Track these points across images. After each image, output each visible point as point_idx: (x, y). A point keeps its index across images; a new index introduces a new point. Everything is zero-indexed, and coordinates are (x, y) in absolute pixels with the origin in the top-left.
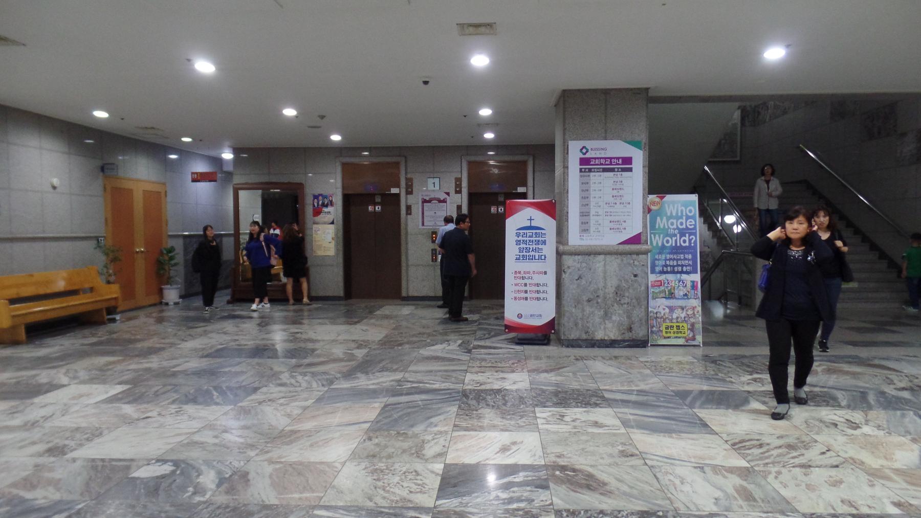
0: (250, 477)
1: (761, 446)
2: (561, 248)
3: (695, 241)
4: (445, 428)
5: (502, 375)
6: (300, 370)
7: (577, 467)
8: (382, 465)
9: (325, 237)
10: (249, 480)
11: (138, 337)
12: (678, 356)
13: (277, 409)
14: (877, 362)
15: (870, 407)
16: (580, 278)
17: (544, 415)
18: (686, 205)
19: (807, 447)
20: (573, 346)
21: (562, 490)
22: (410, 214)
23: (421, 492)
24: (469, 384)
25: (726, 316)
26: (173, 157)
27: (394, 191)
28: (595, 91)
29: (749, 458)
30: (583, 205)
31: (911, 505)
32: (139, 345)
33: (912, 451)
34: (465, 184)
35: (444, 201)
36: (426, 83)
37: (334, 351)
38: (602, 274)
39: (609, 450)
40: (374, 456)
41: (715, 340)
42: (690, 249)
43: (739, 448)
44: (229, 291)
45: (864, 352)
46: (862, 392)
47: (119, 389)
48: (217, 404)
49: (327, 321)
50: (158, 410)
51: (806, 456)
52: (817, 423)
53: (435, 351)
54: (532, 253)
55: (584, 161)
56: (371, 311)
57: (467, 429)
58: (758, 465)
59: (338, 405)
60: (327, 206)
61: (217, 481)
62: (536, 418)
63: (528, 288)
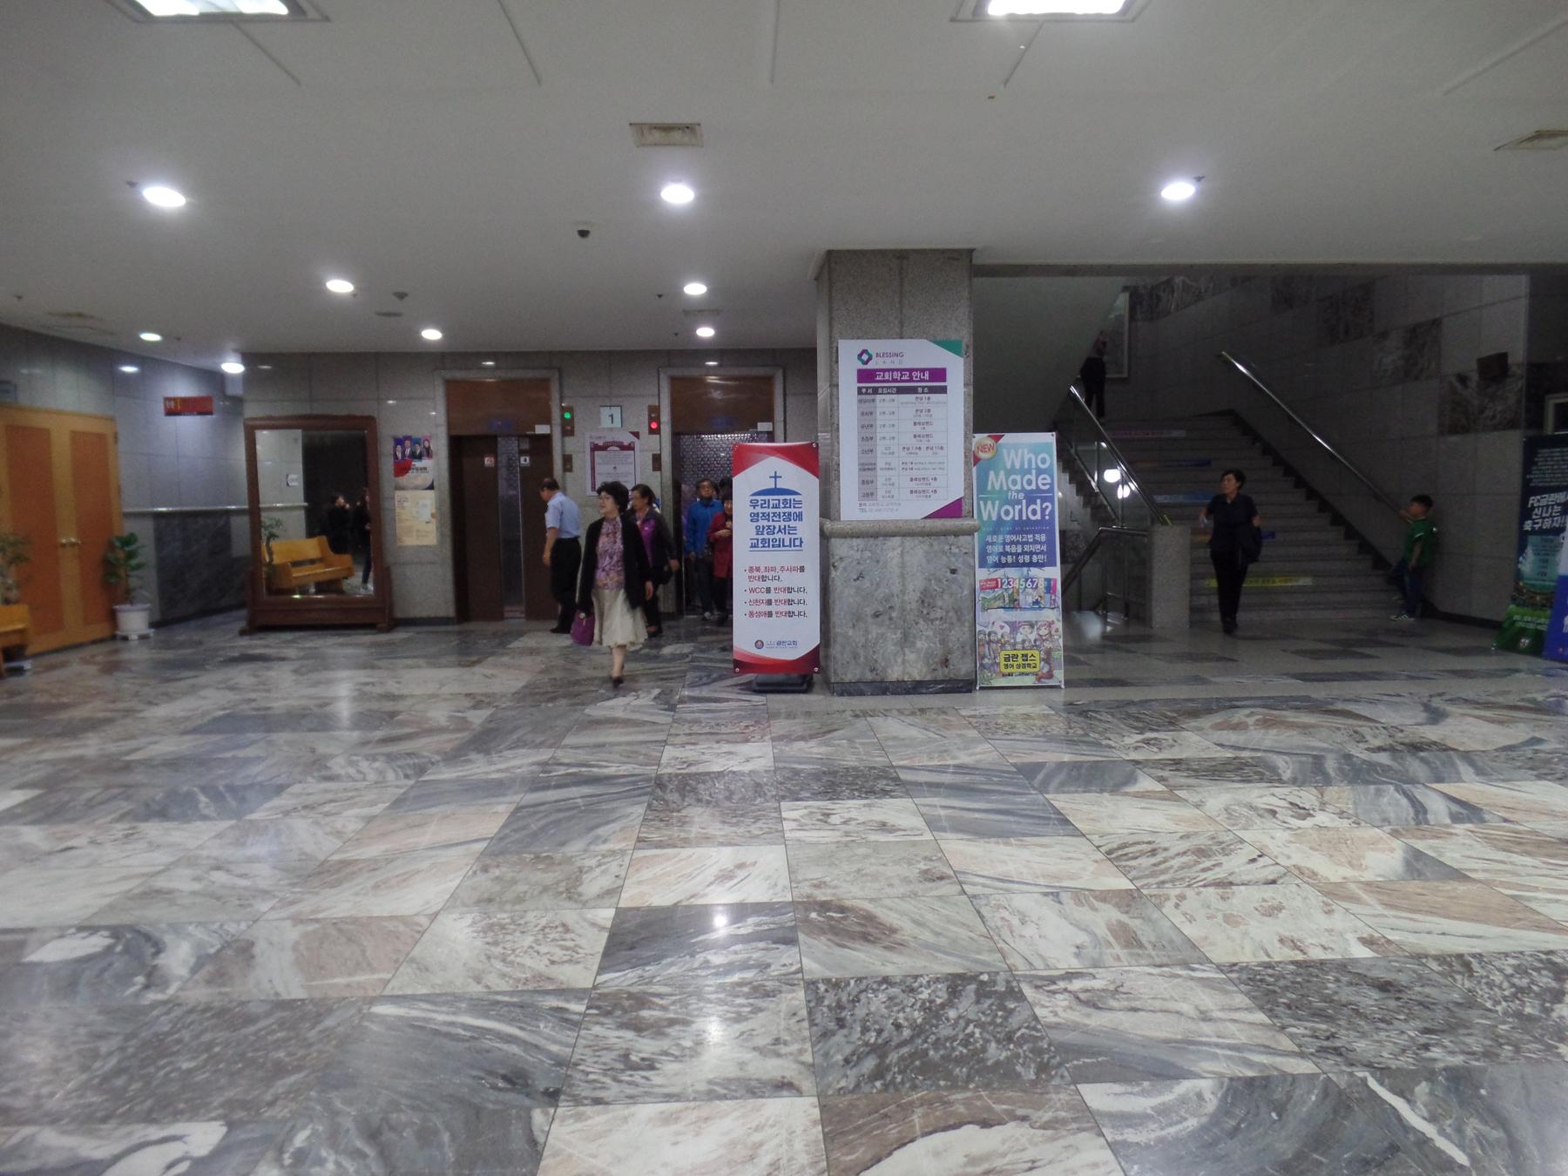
0: (256, 950)
1: (1153, 852)
2: (828, 525)
3: (1052, 512)
4: (622, 845)
5: (726, 747)
6: (367, 750)
7: (848, 903)
8: (503, 917)
9: (417, 513)
10: (253, 957)
11: (65, 700)
12: (1025, 705)
13: (317, 823)
14: (1339, 706)
15: (1328, 781)
16: (860, 576)
17: (794, 814)
18: (1036, 450)
19: (1226, 851)
20: (850, 694)
21: (821, 944)
22: (570, 470)
23: (570, 961)
24: (668, 765)
25: (1105, 636)
26: (129, 369)
27: (541, 429)
28: (882, 253)
29: (1134, 873)
30: (864, 452)
31: (1389, 941)
32: (64, 715)
33: (1392, 850)
34: (665, 417)
35: (630, 447)
36: (583, 234)
37: (431, 714)
38: (897, 571)
39: (903, 870)
40: (490, 900)
41: (1087, 676)
42: (1043, 525)
43: (1118, 858)
44: (244, 613)
45: (1319, 691)
46: (1315, 757)
47: (19, 797)
48: (205, 818)
49: (421, 662)
50: (91, 833)
51: (1225, 867)
52: (1244, 811)
53: (612, 708)
54: (780, 536)
55: (865, 376)
56: (504, 639)
57: (660, 845)
58: (1148, 886)
59: (434, 810)
60: (420, 457)
61: (193, 960)
62: (781, 820)
63: (772, 596)
